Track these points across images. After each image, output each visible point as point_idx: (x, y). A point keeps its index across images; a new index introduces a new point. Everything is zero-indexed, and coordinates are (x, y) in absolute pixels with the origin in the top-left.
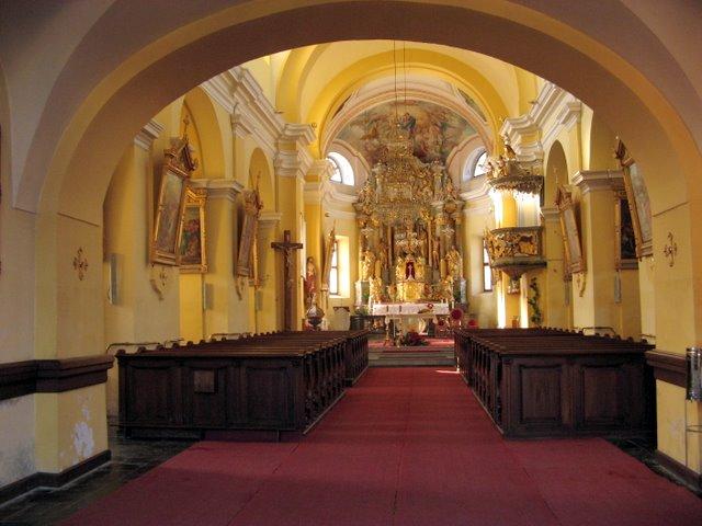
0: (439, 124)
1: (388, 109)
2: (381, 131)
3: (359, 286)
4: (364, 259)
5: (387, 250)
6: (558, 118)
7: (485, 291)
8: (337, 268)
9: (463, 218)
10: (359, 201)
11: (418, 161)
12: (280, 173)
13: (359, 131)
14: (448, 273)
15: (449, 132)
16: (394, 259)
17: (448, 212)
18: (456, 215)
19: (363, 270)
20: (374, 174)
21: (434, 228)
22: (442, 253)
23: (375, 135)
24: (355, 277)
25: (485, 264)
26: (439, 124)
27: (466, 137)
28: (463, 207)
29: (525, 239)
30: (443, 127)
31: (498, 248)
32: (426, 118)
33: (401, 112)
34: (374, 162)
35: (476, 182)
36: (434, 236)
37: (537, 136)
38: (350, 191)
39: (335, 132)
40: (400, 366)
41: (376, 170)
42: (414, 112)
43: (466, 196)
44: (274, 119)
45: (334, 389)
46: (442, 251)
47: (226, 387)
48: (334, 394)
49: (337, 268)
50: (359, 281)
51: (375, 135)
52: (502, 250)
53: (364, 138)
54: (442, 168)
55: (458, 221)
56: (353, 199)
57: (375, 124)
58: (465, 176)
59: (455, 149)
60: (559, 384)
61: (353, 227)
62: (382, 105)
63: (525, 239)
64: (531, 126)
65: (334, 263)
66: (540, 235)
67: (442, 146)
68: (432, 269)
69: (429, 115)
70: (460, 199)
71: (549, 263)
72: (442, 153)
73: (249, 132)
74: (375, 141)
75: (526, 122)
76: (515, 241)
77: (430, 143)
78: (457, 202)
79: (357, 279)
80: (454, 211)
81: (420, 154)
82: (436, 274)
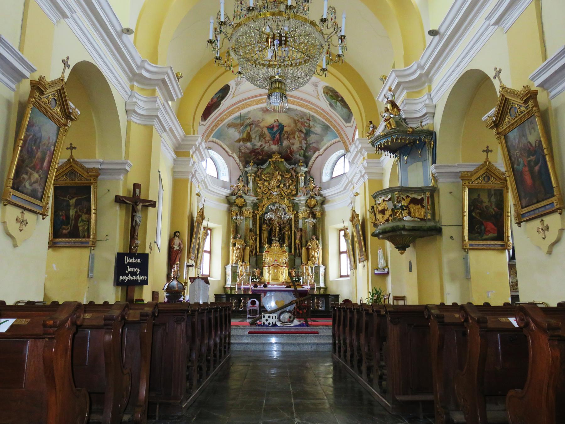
0: (305, 131)
1: (260, 114)
2: (253, 136)
3: (229, 270)
4: (234, 245)
5: (256, 239)
6: (488, 18)
7: (341, 276)
8: (210, 252)
9: (323, 213)
10: (232, 194)
11: (285, 163)
12: (134, 119)
13: (234, 134)
14: (308, 259)
15: (312, 138)
16: (261, 247)
17: (311, 208)
18: (317, 209)
19: (234, 255)
20: (246, 173)
21: (297, 221)
22: (304, 242)
23: (248, 139)
24: (226, 262)
25: (341, 253)
26: (305, 131)
27: (327, 141)
28: (323, 203)
29: (414, 201)
30: (308, 133)
31: (383, 212)
32: (293, 125)
33: (270, 120)
34: (246, 163)
35: (333, 180)
36: (297, 227)
37: (426, 91)
38: (224, 185)
39: (212, 130)
40: (117, 72)
41: (248, 169)
42: (284, 119)
43: (325, 192)
44: (122, 41)
45: (208, 361)
46: (304, 240)
47: (191, 350)
48: (215, 361)
49: (210, 252)
50: (230, 265)
51: (248, 139)
52: (388, 213)
53: (239, 141)
54: (306, 170)
55: (318, 215)
56: (227, 192)
57: (248, 129)
58: (325, 178)
59: (317, 154)
60: (293, 344)
61: (226, 218)
62: (255, 110)
63: (414, 201)
64: (420, 76)
65: (207, 247)
66: (432, 197)
67: (305, 151)
68: (295, 256)
69: (296, 122)
70: (320, 195)
71: (443, 227)
72: (305, 156)
73: (64, 16)
74: (249, 144)
75: (414, 72)
76: (404, 203)
77: (295, 147)
78: (318, 198)
79: (228, 263)
80: (315, 206)
81: (288, 157)
82: (298, 261)
